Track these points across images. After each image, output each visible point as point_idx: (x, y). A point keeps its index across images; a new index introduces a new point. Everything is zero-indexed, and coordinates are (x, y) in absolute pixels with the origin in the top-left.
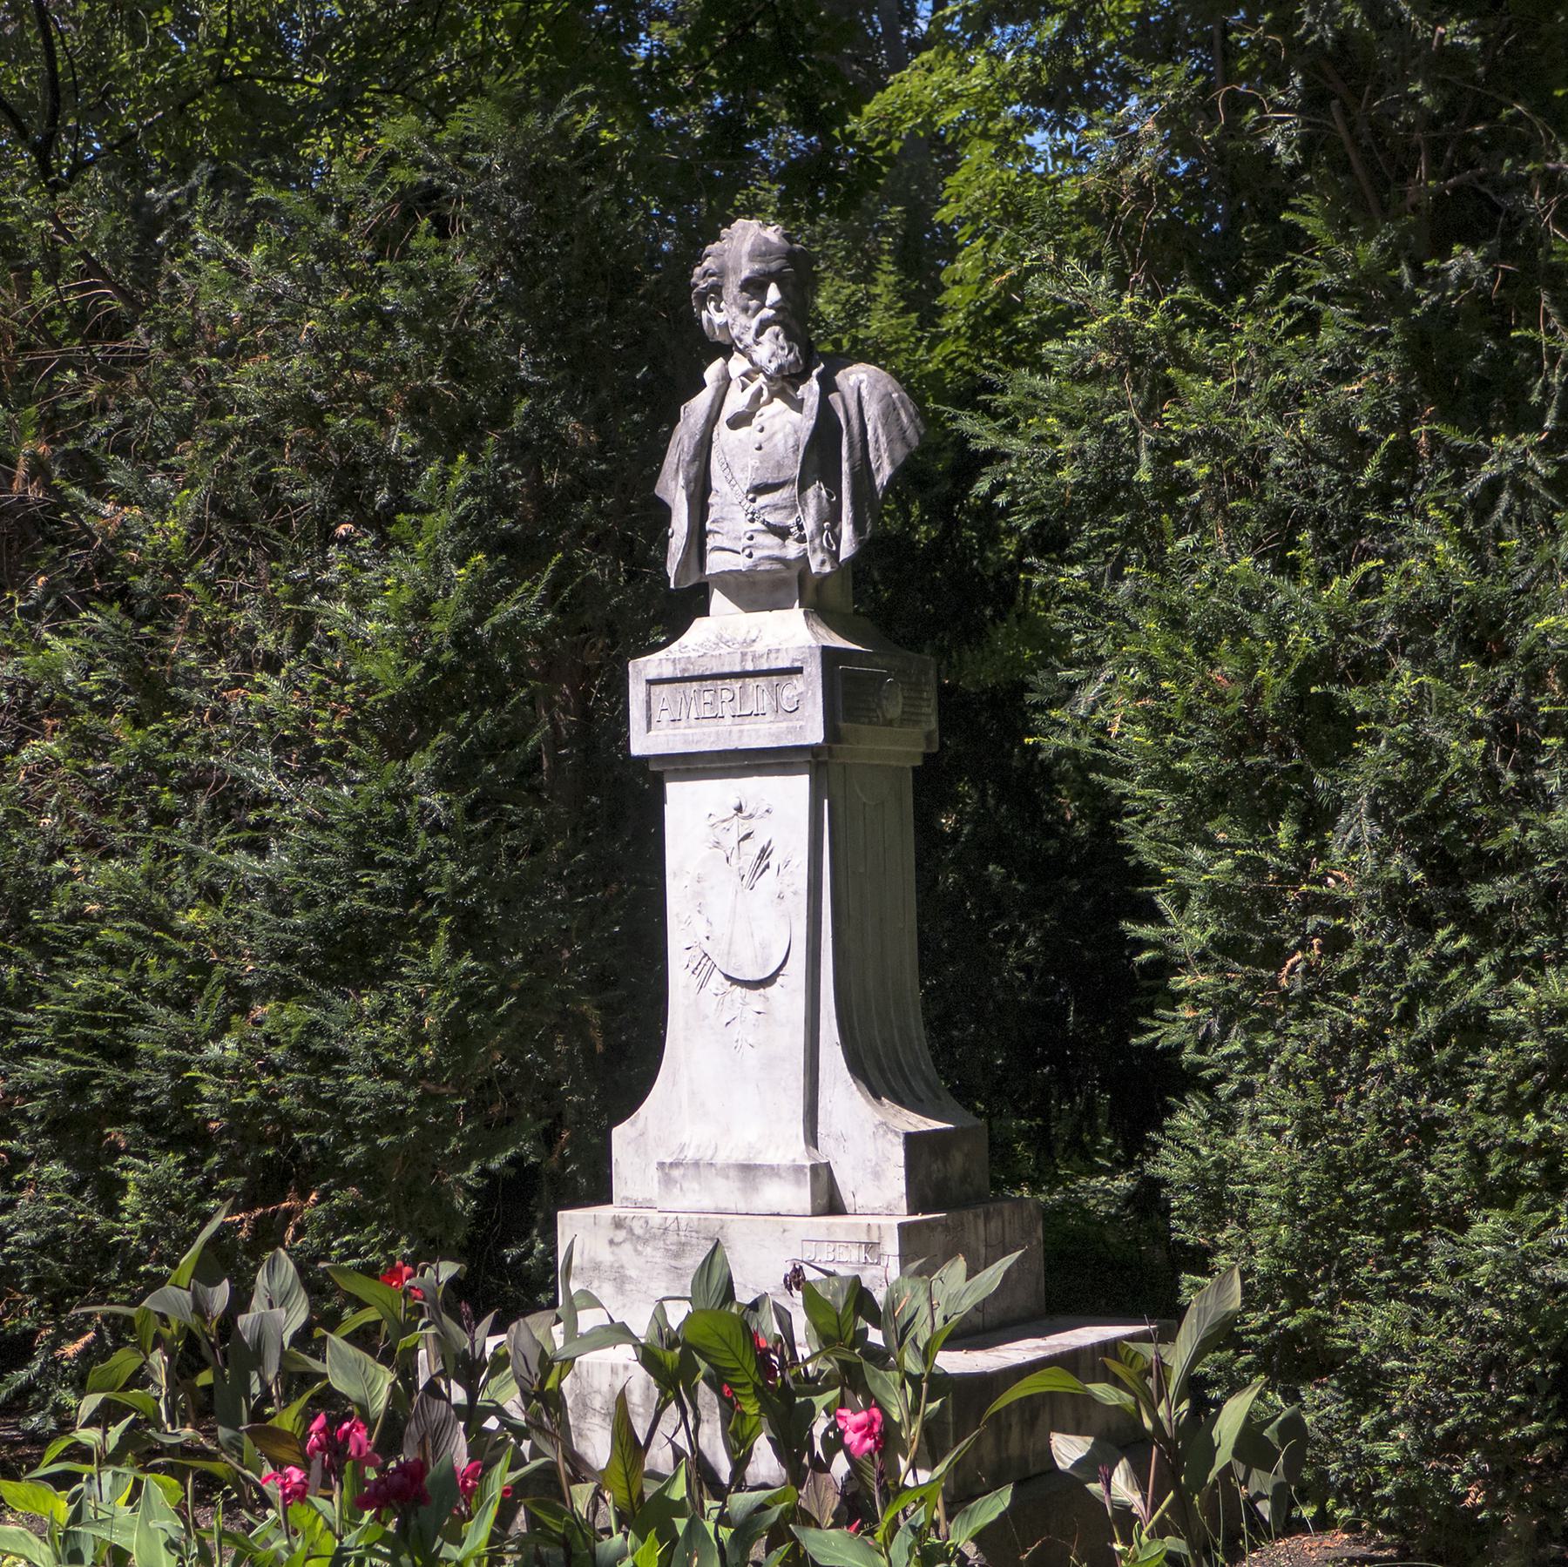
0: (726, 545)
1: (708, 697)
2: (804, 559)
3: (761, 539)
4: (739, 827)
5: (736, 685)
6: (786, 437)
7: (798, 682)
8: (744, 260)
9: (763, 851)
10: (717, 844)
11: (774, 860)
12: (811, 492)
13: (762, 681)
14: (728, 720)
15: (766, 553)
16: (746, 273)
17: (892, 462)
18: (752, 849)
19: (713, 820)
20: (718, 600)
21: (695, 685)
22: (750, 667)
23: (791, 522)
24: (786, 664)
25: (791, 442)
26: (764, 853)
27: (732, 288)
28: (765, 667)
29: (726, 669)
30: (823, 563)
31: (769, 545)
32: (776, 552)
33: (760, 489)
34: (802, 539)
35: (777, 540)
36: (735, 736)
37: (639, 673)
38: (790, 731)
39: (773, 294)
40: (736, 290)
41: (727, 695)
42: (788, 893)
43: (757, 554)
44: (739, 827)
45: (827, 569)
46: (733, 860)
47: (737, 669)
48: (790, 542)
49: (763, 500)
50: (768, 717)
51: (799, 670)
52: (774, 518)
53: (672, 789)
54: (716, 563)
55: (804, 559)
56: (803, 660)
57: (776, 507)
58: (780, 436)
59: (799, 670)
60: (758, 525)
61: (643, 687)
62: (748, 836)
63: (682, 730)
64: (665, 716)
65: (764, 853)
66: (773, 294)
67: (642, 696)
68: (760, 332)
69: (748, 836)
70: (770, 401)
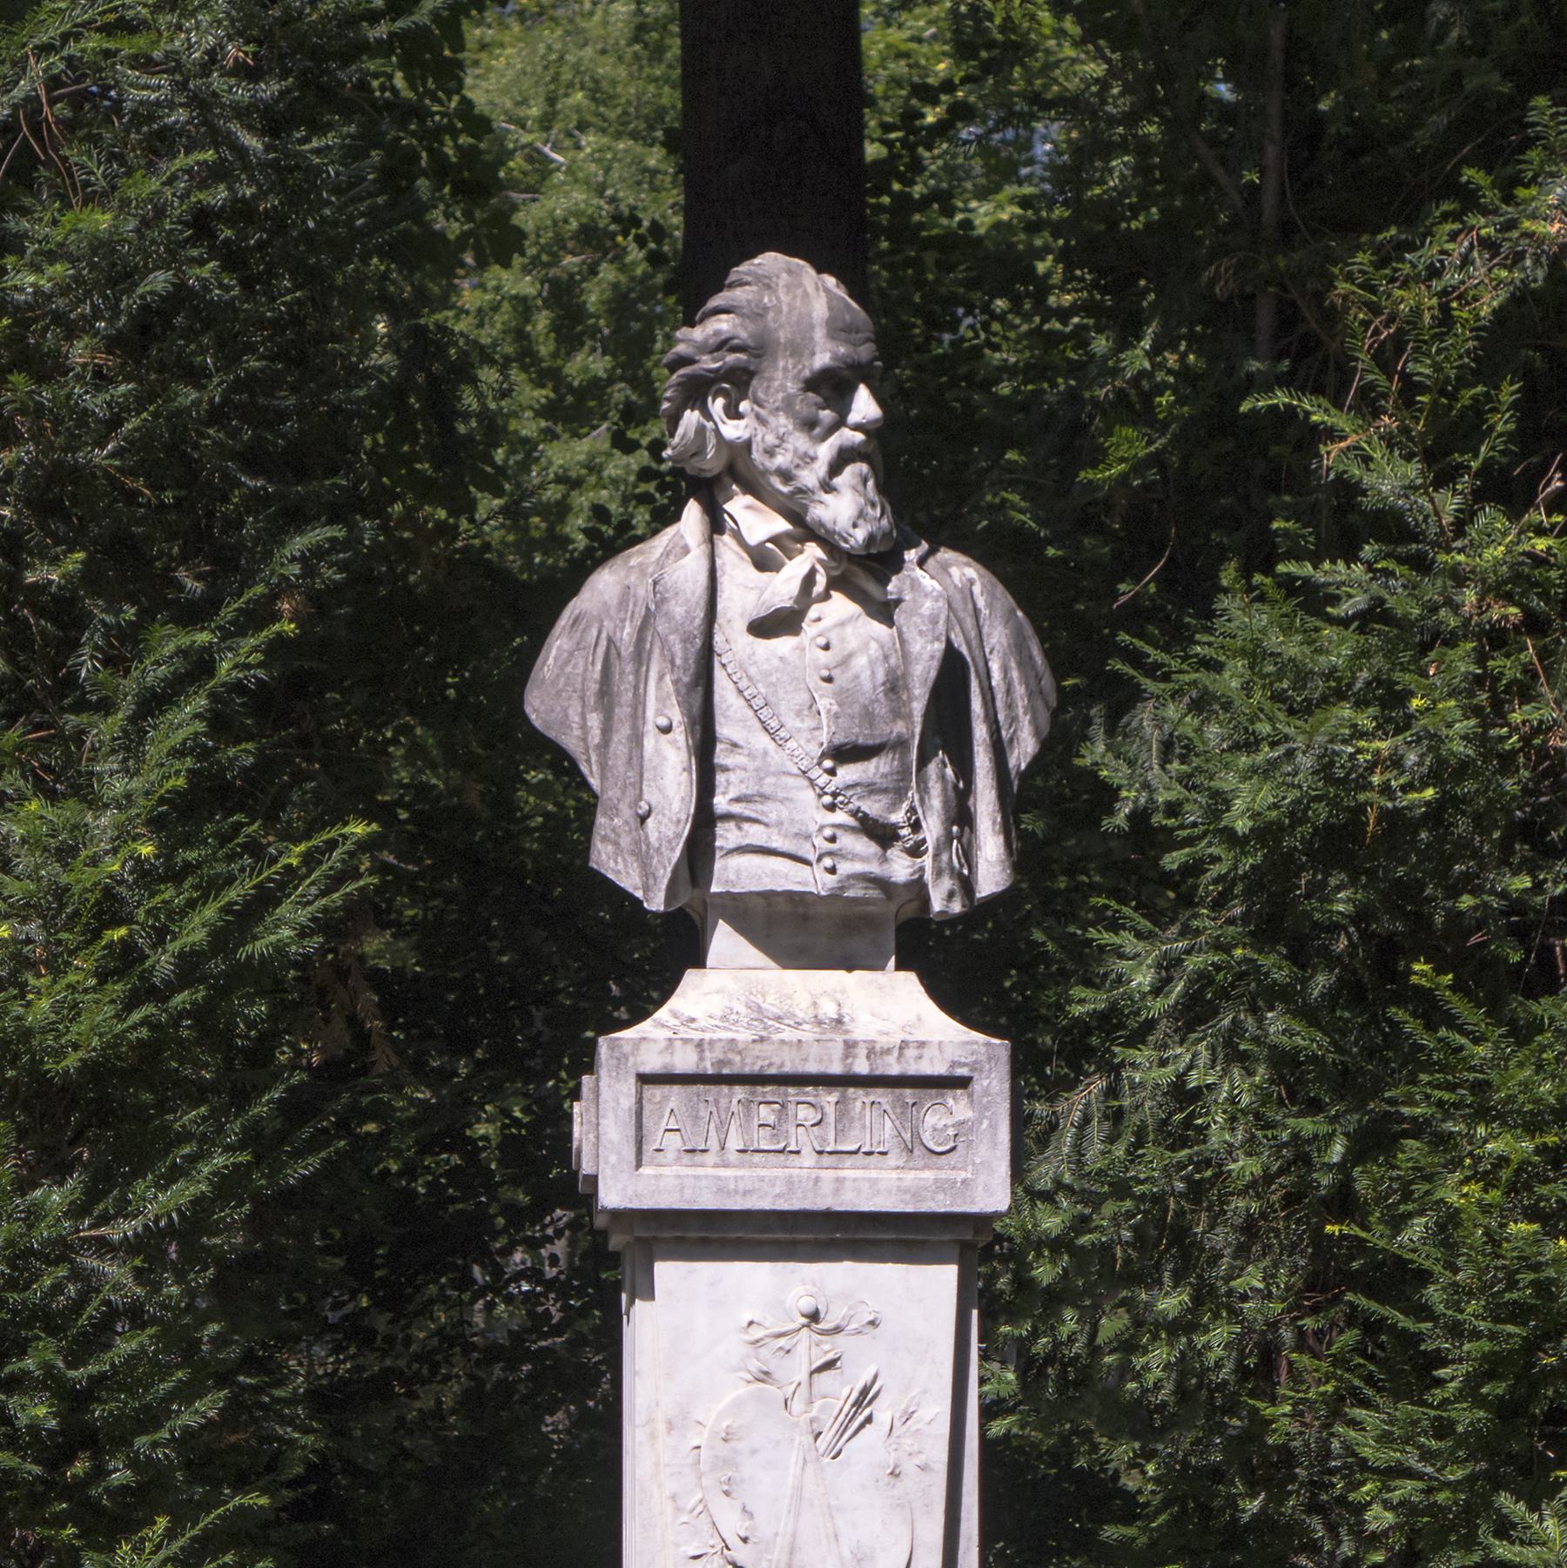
0: (777, 843)
1: (766, 1114)
2: (918, 888)
3: (850, 842)
4: (809, 1349)
5: (829, 1098)
6: (872, 664)
7: (958, 1106)
8: (819, 334)
9: (865, 1391)
10: (765, 1376)
11: (883, 1412)
12: (932, 768)
13: (882, 1096)
14: (808, 1158)
15: (859, 867)
16: (822, 359)
17: (1037, 732)
18: (840, 1389)
19: (756, 1333)
20: (725, 941)
21: (740, 1092)
22: (862, 1067)
23: (898, 817)
24: (939, 1068)
25: (881, 676)
26: (865, 1397)
27: (782, 379)
28: (895, 1070)
29: (812, 1068)
30: (951, 895)
31: (861, 854)
32: (874, 868)
33: (844, 753)
34: (916, 851)
35: (872, 848)
36: (826, 1187)
37: (622, 1059)
38: (941, 1186)
39: (864, 406)
40: (792, 387)
41: (804, 1113)
42: (909, 1467)
43: (845, 868)
44: (809, 1349)
45: (957, 907)
46: (797, 1406)
47: (836, 1068)
48: (895, 853)
49: (849, 773)
50: (892, 1160)
51: (963, 1083)
52: (873, 807)
53: (666, 1272)
54: (734, 873)
55: (918, 888)
56: (974, 1066)
57: (871, 789)
58: (861, 662)
59: (963, 1083)
60: (841, 817)
61: (630, 1085)
62: (829, 1365)
63: (708, 1170)
64: (674, 1142)
65: (865, 1397)
66: (864, 406)
67: (628, 1102)
68: (836, 468)
69: (829, 1365)
70: (826, 596)
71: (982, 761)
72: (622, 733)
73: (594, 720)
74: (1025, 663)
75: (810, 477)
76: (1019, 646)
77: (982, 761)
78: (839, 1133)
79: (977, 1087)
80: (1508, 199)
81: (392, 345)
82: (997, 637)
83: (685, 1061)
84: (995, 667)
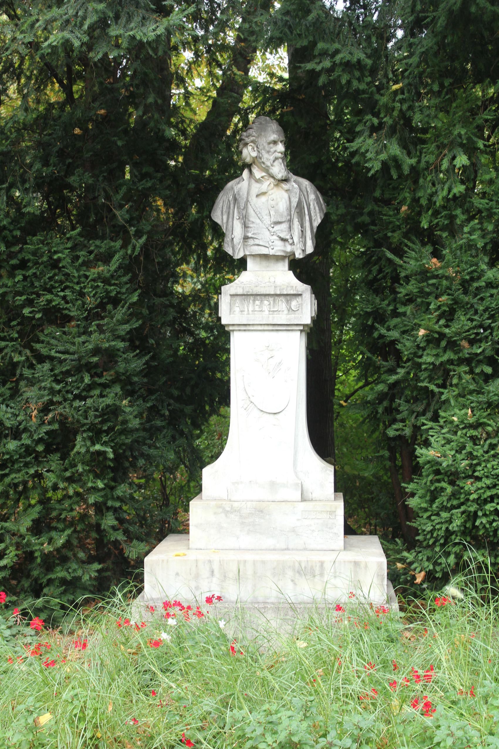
5: (271, 299)
13: (282, 298)
14: (267, 312)
24: (295, 292)
47: (272, 293)
49: (277, 228)
71: (307, 224)
72: (230, 220)
73: (225, 217)
74: (319, 203)
75: (269, 164)
76: (317, 198)
77: (307, 224)
78: (274, 307)
79: (304, 296)
80: (60, 269)
81: (199, 360)
82: (312, 197)
83: (240, 292)
84: (311, 204)
